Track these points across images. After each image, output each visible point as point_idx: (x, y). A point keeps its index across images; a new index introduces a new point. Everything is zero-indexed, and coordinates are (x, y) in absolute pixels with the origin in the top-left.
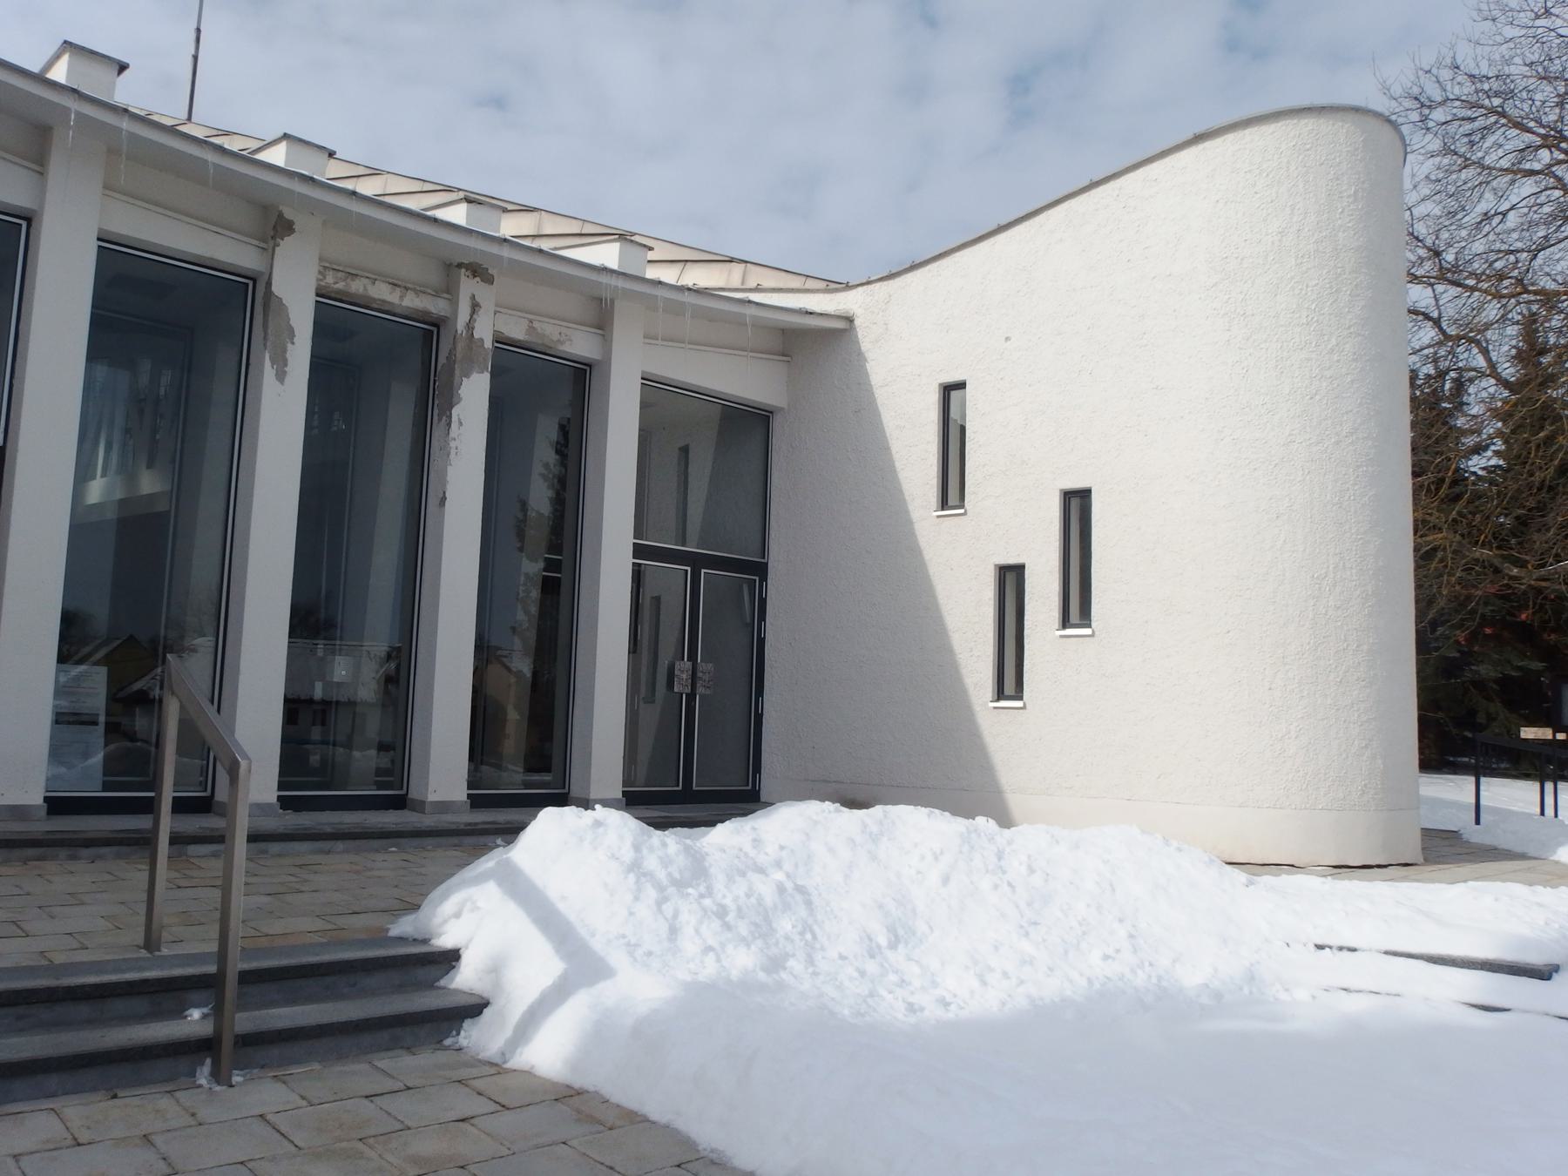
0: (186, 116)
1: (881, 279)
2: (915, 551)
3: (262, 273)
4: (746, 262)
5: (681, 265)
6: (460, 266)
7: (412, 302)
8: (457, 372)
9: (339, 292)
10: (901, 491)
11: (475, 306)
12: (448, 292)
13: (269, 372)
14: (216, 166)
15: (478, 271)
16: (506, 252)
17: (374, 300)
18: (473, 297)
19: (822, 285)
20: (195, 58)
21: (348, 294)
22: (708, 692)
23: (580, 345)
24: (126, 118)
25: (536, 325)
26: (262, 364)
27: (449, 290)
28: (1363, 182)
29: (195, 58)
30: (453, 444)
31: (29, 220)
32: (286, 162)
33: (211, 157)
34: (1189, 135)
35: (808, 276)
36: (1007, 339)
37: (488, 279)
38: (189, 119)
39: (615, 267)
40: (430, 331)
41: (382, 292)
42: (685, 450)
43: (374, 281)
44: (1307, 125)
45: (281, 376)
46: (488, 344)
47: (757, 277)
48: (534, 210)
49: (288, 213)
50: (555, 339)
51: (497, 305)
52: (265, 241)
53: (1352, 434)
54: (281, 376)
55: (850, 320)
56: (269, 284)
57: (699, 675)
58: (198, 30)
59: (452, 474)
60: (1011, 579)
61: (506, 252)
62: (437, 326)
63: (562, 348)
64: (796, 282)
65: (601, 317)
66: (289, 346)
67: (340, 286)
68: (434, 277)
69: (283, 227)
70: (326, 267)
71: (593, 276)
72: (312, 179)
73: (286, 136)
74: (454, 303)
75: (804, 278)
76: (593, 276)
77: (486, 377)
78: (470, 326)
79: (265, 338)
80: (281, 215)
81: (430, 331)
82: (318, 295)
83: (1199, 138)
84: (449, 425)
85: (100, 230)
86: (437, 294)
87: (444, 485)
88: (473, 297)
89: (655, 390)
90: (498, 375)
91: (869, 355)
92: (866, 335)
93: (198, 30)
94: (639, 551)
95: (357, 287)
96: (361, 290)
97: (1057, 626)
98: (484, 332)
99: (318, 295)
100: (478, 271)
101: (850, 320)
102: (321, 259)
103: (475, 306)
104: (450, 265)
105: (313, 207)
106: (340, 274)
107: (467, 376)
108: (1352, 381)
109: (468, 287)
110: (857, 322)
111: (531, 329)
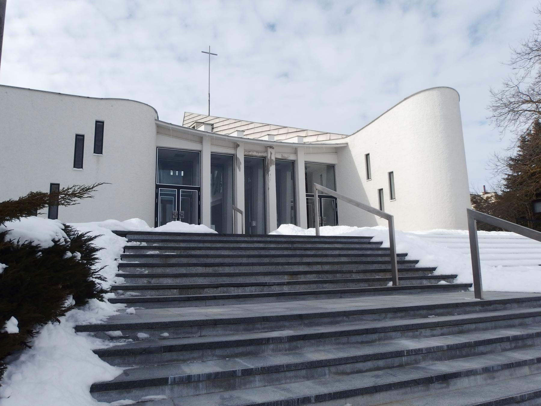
0: (208, 114)
1: (352, 135)
2: (363, 189)
3: (235, 154)
4: (330, 133)
5: (317, 135)
6: (268, 147)
7: (260, 154)
8: (269, 166)
9: (248, 155)
10: (360, 177)
11: (271, 154)
12: (266, 152)
13: (238, 170)
14: (227, 139)
15: (271, 147)
16: (275, 143)
17: (253, 155)
18: (271, 152)
19: (345, 136)
20: (209, 100)
21: (249, 155)
22: (325, 223)
23: (292, 157)
24: (214, 134)
25: (283, 155)
26: (236, 168)
27: (266, 151)
28: (441, 102)
29: (209, 100)
30: (269, 179)
31: (200, 152)
32: (237, 135)
33: (226, 137)
34: (403, 99)
35: (342, 135)
36: (376, 144)
37: (273, 148)
38: (209, 115)
39: (297, 142)
40: (264, 159)
41: (255, 154)
42: (321, 175)
43: (253, 152)
44: (427, 93)
45: (240, 170)
46: (274, 160)
47: (333, 137)
48: (287, 127)
49: (238, 143)
50: (287, 157)
51: (275, 152)
52: (235, 148)
53: (442, 153)
54: (240, 170)
55: (347, 144)
56: (236, 155)
57: (323, 219)
58: (209, 94)
59: (270, 184)
60: (381, 191)
61: (275, 143)
62: (265, 158)
63: (288, 158)
64: (340, 137)
65: (296, 153)
66: (241, 165)
67: (248, 154)
68: (263, 149)
69: (238, 146)
70: (245, 151)
71: (291, 145)
72: (242, 138)
73: (237, 130)
74: (267, 153)
75: (341, 135)
76: (291, 145)
77: (275, 166)
78: (271, 157)
79: (237, 164)
80: (237, 144)
81: (264, 159)
82: (244, 156)
83: (405, 99)
84: (269, 175)
85: (211, 151)
86: (264, 152)
87: (269, 186)
88: (271, 152)
89: (307, 165)
90: (277, 165)
91: (351, 151)
92: (351, 147)
93: (209, 94)
94: (307, 196)
95: (250, 153)
96: (251, 154)
97: (389, 199)
98: (273, 158)
99: (244, 156)
100: (271, 147)
101: (347, 144)
102: (244, 150)
103: (271, 154)
104: (266, 147)
105: (242, 142)
106: (247, 152)
107: (271, 166)
108: (441, 142)
109: (270, 150)
110: (349, 144)
111: (282, 156)
